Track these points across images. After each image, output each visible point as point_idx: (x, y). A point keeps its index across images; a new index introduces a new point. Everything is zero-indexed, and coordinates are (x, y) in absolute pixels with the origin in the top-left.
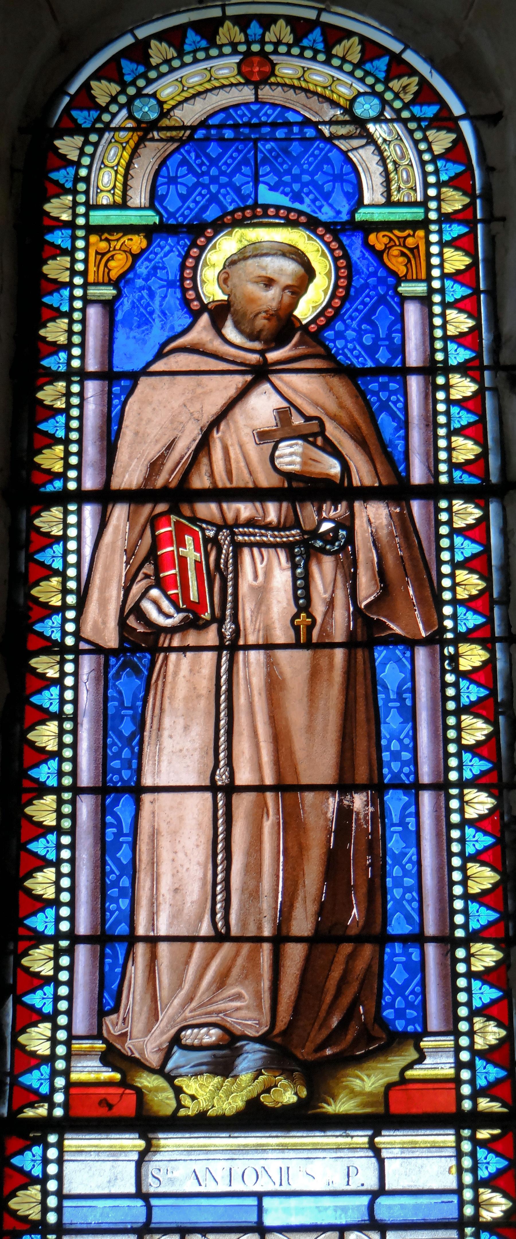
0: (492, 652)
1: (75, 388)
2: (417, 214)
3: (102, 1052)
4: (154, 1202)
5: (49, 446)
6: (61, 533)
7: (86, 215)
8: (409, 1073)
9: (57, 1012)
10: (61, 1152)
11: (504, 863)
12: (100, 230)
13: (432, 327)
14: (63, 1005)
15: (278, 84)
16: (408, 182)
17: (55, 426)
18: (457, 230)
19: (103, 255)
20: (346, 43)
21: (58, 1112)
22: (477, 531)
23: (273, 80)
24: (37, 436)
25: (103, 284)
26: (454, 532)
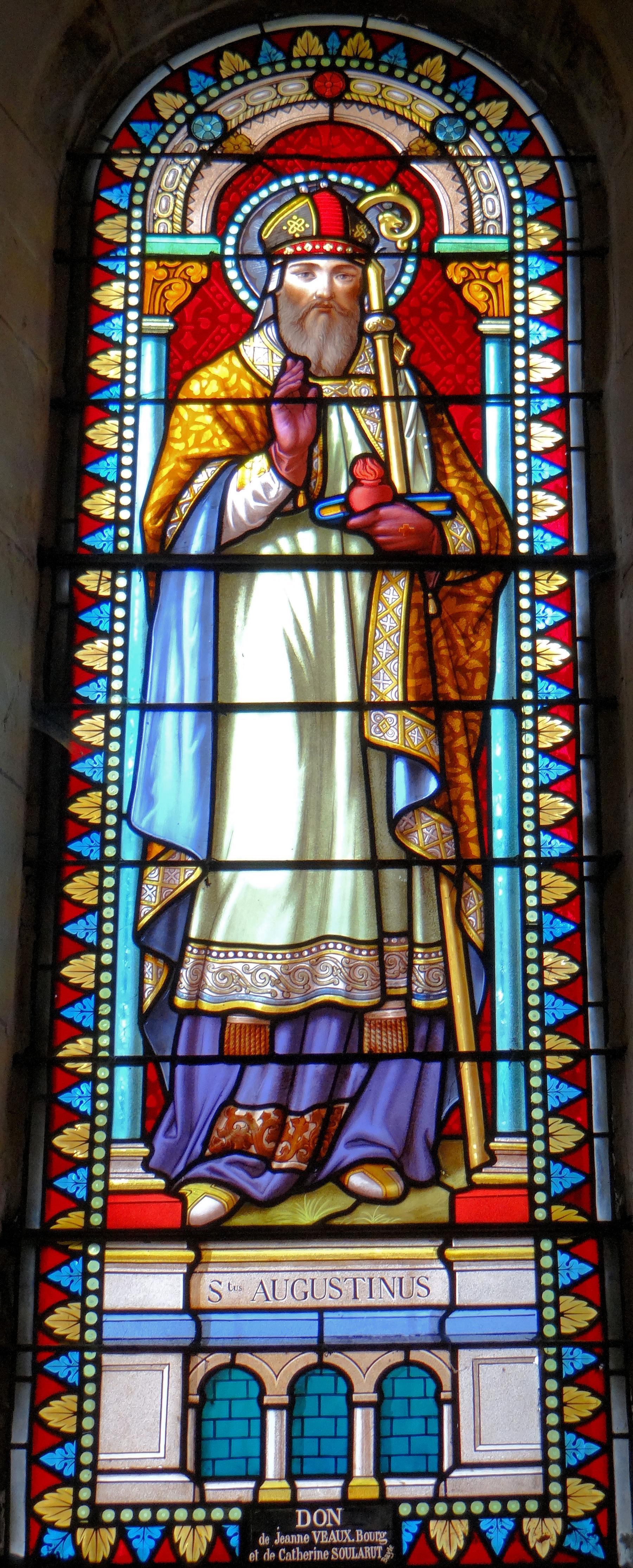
1: (109, 882)
2: (501, 245)
4: (202, 1317)
5: (99, 490)
9: (95, 1112)
12: (158, 258)
13: (522, 818)
14: (108, 897)
15: (352, 102)
16: (489, 185)
17: (105, 469)
22: (561, 599)
23: (347, 96)
24: (57, 1110)
25: (159, 316)
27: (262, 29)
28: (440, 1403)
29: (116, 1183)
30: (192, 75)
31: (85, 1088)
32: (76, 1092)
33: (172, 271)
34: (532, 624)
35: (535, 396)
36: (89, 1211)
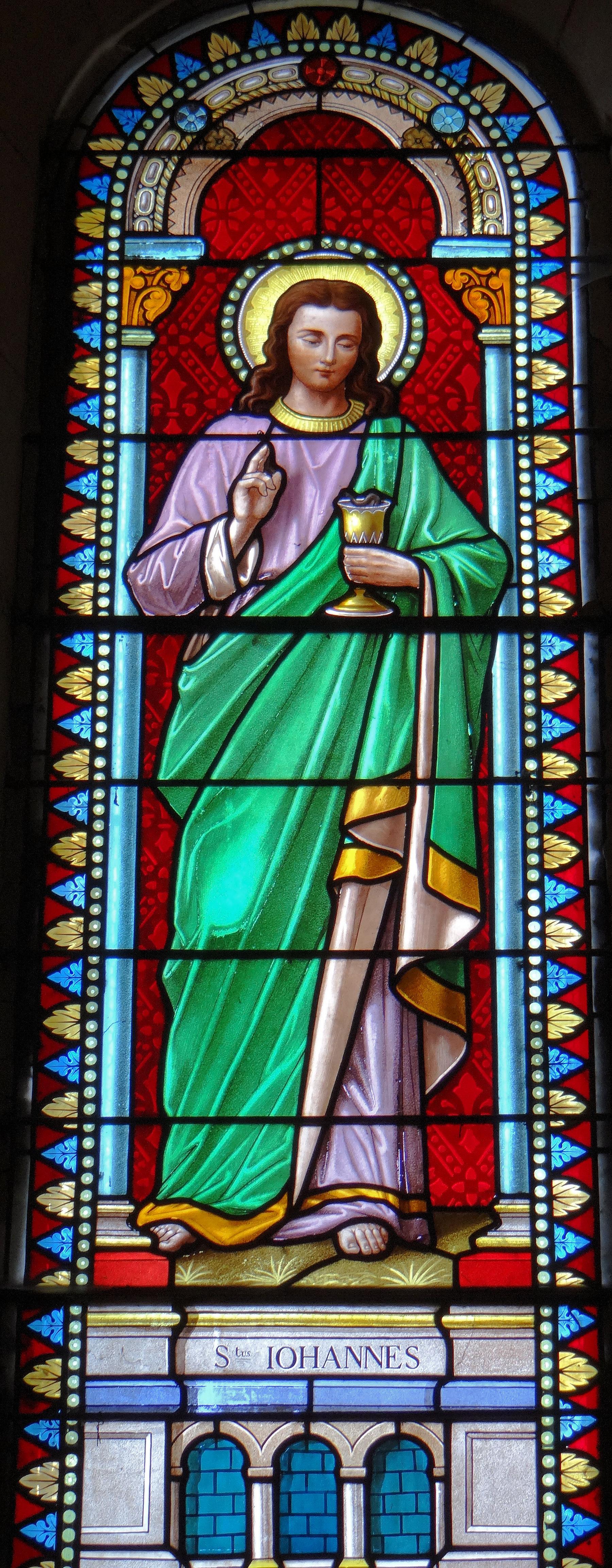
0: (571, 444)
2: (500, 251)
3: (130, 1214)
6: (97, 386)
7: (81, 1391)
8: (482, 1241)
9: (98, 657)
10: (85, 1328)
11: (601, 1348)
13: (518, 484)
16: (488, 181)
18: (548, 268)
19: (139, 292)
20: (419, 45)
21: (82, 1280)
26: (534, 468)
27: (251, 10)
28: (433, 1480)
29: (100, 1240)
30: (179, 58)
31: (90, 552)
32: (70, 885)
33: (149, 279)
34: (539, 819)
35: (566, 1413)
36: (75, 1271)
